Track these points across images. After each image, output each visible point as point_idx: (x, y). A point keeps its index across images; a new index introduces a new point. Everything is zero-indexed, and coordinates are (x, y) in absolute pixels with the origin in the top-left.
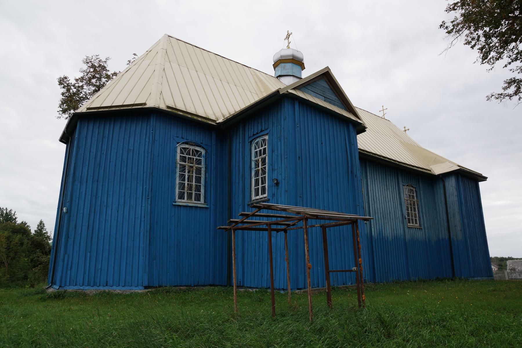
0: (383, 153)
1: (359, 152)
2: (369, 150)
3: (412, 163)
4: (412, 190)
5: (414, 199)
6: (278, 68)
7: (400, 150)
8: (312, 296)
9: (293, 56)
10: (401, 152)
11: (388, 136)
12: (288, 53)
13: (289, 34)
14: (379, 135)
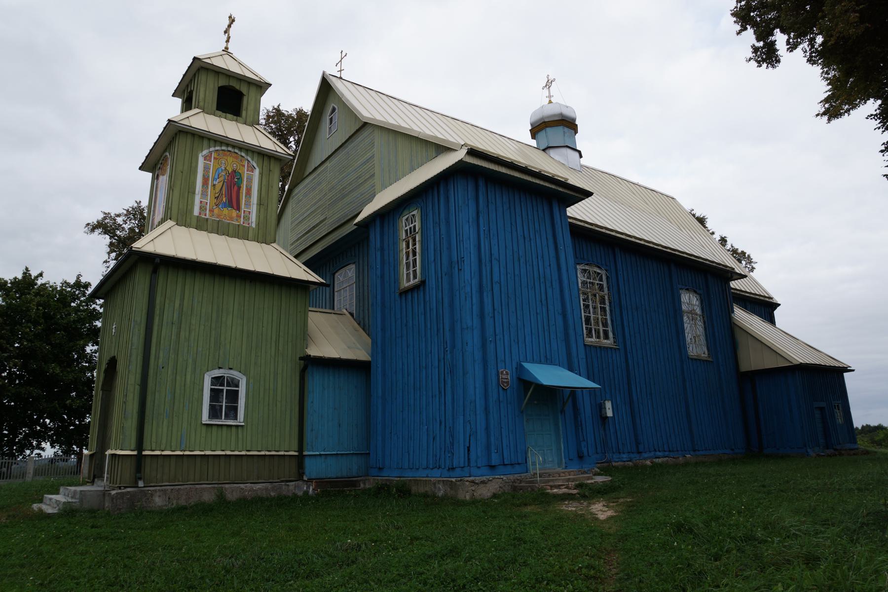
0: (618, 227)
1: (570, 223)
2: (602, 223)
3: (629, 231)
4: (599, 274)
5: (603, 291)
6: (541, 135)
7: (609, 207)
8: (769, 557)
9: (561, 114)
10: (644, 219)
11: (650, 204)
12: (551, 111)
13: (547, 87)
14: (649, 210)
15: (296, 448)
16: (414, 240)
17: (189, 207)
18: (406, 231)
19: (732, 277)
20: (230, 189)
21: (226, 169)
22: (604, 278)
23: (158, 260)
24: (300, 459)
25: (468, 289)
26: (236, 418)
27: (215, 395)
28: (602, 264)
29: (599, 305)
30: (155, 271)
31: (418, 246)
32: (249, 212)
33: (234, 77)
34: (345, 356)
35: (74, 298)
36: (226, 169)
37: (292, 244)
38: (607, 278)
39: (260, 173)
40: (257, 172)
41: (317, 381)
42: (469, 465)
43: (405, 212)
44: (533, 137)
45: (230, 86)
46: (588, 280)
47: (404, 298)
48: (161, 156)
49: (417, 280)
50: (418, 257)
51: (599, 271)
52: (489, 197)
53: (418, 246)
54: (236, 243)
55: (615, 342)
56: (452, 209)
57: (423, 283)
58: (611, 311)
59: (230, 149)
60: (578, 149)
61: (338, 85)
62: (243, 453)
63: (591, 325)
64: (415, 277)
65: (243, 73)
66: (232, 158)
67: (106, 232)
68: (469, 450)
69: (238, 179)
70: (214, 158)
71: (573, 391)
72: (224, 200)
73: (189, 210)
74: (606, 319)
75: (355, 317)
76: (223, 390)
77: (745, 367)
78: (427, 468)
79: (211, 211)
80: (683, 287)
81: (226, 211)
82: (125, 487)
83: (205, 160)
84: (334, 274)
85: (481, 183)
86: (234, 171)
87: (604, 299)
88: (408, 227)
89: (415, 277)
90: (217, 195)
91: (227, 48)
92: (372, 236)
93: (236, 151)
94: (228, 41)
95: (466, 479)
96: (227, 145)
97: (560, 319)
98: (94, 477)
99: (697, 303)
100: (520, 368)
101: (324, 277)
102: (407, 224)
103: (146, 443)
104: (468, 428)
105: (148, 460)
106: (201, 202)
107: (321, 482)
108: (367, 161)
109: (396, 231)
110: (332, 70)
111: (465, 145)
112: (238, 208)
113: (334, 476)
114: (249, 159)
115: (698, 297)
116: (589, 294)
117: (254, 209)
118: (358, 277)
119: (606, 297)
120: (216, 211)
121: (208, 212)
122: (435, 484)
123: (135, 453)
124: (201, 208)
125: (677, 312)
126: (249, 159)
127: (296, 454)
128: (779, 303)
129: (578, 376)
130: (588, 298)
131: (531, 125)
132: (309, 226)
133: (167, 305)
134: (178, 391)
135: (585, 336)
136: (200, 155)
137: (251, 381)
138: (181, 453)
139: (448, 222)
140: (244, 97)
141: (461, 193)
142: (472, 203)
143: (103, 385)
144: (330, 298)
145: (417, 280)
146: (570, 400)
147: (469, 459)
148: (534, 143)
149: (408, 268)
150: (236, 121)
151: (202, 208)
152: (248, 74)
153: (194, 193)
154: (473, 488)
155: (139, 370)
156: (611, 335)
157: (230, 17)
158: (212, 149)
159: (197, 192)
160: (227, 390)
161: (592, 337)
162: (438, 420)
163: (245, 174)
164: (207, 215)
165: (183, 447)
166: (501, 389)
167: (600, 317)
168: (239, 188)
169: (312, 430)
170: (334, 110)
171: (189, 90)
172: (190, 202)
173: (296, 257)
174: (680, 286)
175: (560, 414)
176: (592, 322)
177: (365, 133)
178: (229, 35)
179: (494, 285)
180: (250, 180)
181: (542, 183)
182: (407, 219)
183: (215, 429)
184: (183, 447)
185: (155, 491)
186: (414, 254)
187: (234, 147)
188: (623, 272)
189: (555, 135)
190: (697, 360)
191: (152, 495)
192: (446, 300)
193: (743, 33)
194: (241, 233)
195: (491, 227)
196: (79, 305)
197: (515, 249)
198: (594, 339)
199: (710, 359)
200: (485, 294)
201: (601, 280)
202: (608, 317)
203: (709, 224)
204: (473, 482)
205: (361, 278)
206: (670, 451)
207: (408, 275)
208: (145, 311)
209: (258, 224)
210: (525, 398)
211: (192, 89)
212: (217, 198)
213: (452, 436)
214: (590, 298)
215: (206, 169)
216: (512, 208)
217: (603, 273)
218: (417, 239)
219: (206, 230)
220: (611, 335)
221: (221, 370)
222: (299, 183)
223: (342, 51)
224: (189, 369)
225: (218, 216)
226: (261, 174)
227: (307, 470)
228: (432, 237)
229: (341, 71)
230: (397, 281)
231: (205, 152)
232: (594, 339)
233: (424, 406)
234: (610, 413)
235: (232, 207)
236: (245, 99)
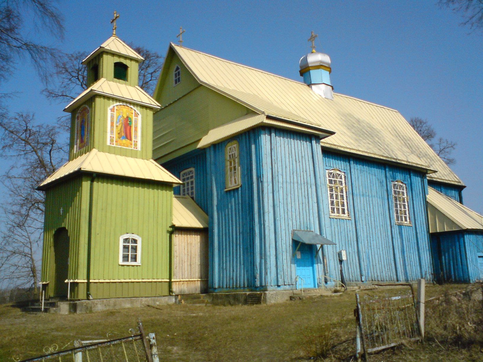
4: (339, 175)
20: (125, 128)
22: (343, 177)
24: (170, 283)
27: (126, 248)
30: (92, 181)
32: (137, 141)
40: (140, 117)
41: (178, 238)
45: (120, 62)
46: (333, 179)
55: (348, 216)
63: (334, 206)
65: (128, 54)
66: (125, 109)
69: (130, 121)
74: (343, 202)
75: (195, 199)
76: (129, 246)
83: (111, 111)
86: (128, 117)
102: (230, 152)
112: (131, 140)
119: (344, 189)
121: (114, 142)
131: (301, 67)
135: (330, 213)
140: (129, 68)
146: (321, 249)
151: (112, 140)
153: (106, 132)
156: (346, 212)
160: (132, 246)
161: (335, 213)
163: (134, 118)
164: (114, 144)
167: (339, 200)
170: (178, 69)
176: (335, 204)
180: (136, 121)
182: (230, 149)
198: (336, 214)
201: (341, 178)
202: (345, 201)
206: (382, 281)
215: (112, 117)
218: (236, 162)
219: (114, 153)
221: (128, 234)
226: (142, 118)
236: (129, 69)
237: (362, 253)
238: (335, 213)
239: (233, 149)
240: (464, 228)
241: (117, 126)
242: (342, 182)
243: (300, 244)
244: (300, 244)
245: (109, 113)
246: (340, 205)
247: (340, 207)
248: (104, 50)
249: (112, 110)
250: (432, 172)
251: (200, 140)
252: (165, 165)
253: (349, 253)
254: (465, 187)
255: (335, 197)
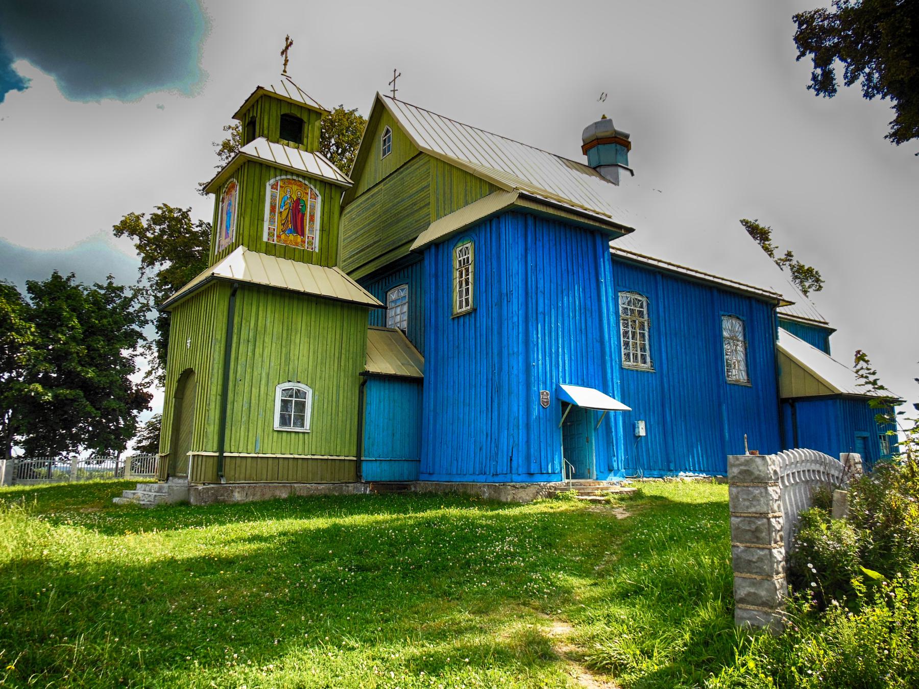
4: (640, 301)
6: (593, 151)
15: (355, 454)
16: (467, 270)
17: (259, 234)
18: (460, 262)
19: (778, 303)
21: (291, 197)
22: (645, 304)
23: (236, 285)
24: (358, 463)
25: (515, 319)
26: (302, 426)
27: (285, 404)
28: (643, 292)
29: (638, 331)
31: (470, 276)
33: (295, 105)
34: (399, 373)
35: (109, 301)
36: (291, 197)
37: (344, 261)
38: (648, 304)
39: (322, 201)
40: (319, 199)
41: (376, 395)
42: (511, 472)
43: (460, 244)
44: (585, 153)
46: (629, 307)
47: (456, 321)
48: (227, 181)
49: (469, 307)
50: (470, 287)
51: (640, 298)
52: (537, 236)
53: (470, 276)
54: (302, 268)
55: (652, 366)
56: (503, 246)
57: (475, 310)
58: (649, 336)
59: (295, 177)
60: (629, 167)
61: (389, 102)
62: (309, 457)
64: (467, 304)
67: (132, 233)
68: (511, 460)
69: (302, 206)
70: (281, 187)
71: (607, 412)
72: (290, 226)
73: (259, 237)
77: (785, 394)
78: (474, 473)
79: (279, 237)
80: (726, 313)
81: (291, 237)
82: (209, 484)
84: (386, 293)
85: (530, 222)
86: (298, 199)
87: (644, 326)
88: (461, 258)
89: (467, 304)
90: (283, 222)
91: (285, 71)
92: (426, 262)
93: (301, 179)
94: (285, 65)
95: (508, 484)
96: (292, 174)
97: (597, 345)
98: (168, 476)
99: (740, 329)
100: (559, 390)
101: (380, 297)
103: (226, 447)
104: (511, 441)
105: (228, 460)
106: (269, 228)
107: (377, 484)
108: (423, 189)
109: (450, 260)
110: (384, 91)
111: (517, 189)
112: (303, 234)
113: (388, 480)
114: (313, 187)
115: (741, 323)
116: (630, 320)
117: (317, 234)
118: (410, 297)
120: (283, 237)
121: (275, 238)
122: (480, 488)
123: (217, 454)
124: (269, 234)
125: (717, 340)
126: (313, 187)
127: (355, 459)
128: (830, 326)
129: (612, 399)
130: (628, 324)
131: (583, 141)
132: (363, 245)
133: (243, 324)
134: (253, 401)
136: (267, 184)
137: (317, 393)
138: (256, 455)
139: (499, 258)
141: (509, 232)
142: (521, 242)
143: (176, 393)
144: (382, 315)
145: (469, 307)
147: (511, 467)
148: (584, 160)
149: (461, 297)
150: (298, 148)
152: (309, 102)
153: (263, 220)
154: (514, 492)
155: (220, 382)
156: (648, 359)
157: (287, 39)
158: (278, 178)
159: (265, 219)
162: (485, 433)
165: (257, 450)
166: (541, 407)
167: (638, 342)
168: (303, 215)
169: (369, 438)
170: (388, 131)
171: (251, 115)
172: (259, 229)
173: (348, 274)
174: (722, 313)
175: (593, 431)
177: (421, 162)
178: (286, 57)
179: (539, 315)
180: (313, 208)
181: (586, 221)
183: (284, 434)
184: (257, 450)
185: (235, 487)
186: (467, 284)
187: (298, 175)
188: (664, 299)
189: (607, 153)
190: (736, 385)
191: (232, 491)
192: (495, 328)
193: (802, 59)
194: (305, 257)
195: (538, 263)
196: (114, 308)
197: (559, 283)
199: (749, 385)
200: (530, 324)
201: (642, 307)
202: (647, 342)
203: (775, 239)
204: (514, 486)
205: (414, 298)
207: (461, 302)
208: (224, 331)
209: (321, 249)
210: (563, 414)
211: (255, 114)
212: (283, 224)
213: (497, 446)
214: (630, 323)
215: (273, 197)
216: (558, 244)
217: (644, 300)
218: (470, 271)
219: (275, 255)
220: (648, 359)
222: (351, 202)
223: (395, 70)
224: (263, 382)
225: (285, 241)
226: (323, 202)
227: (364, 475)
228: (484, 270)
229: (394, 91)
230: (450, 306)
231: (272, 181)
232: (631, 363)
233: (473, 419)
234: (642, 433)
235: (297, 233)
237: (521, 404)
238: (630, 361)
239: (464, 252)
240: (836, 392)
241: (281, 213)
242: (643, 312)
243: (570, 407)
244: (570, 407)
245: (268, 188)
246: (639, 349)
247: (639, 353)
248: (265, 93)
249: (274, 187)
250: (785, 303)
251: (416, 238)
252: (361, 282)
253: (731, 397)
254: (833, 330)
255: (630, 336)
